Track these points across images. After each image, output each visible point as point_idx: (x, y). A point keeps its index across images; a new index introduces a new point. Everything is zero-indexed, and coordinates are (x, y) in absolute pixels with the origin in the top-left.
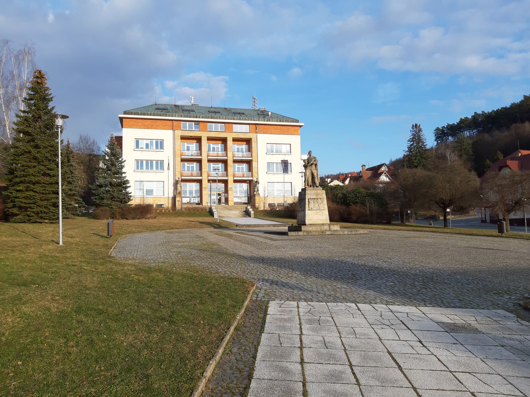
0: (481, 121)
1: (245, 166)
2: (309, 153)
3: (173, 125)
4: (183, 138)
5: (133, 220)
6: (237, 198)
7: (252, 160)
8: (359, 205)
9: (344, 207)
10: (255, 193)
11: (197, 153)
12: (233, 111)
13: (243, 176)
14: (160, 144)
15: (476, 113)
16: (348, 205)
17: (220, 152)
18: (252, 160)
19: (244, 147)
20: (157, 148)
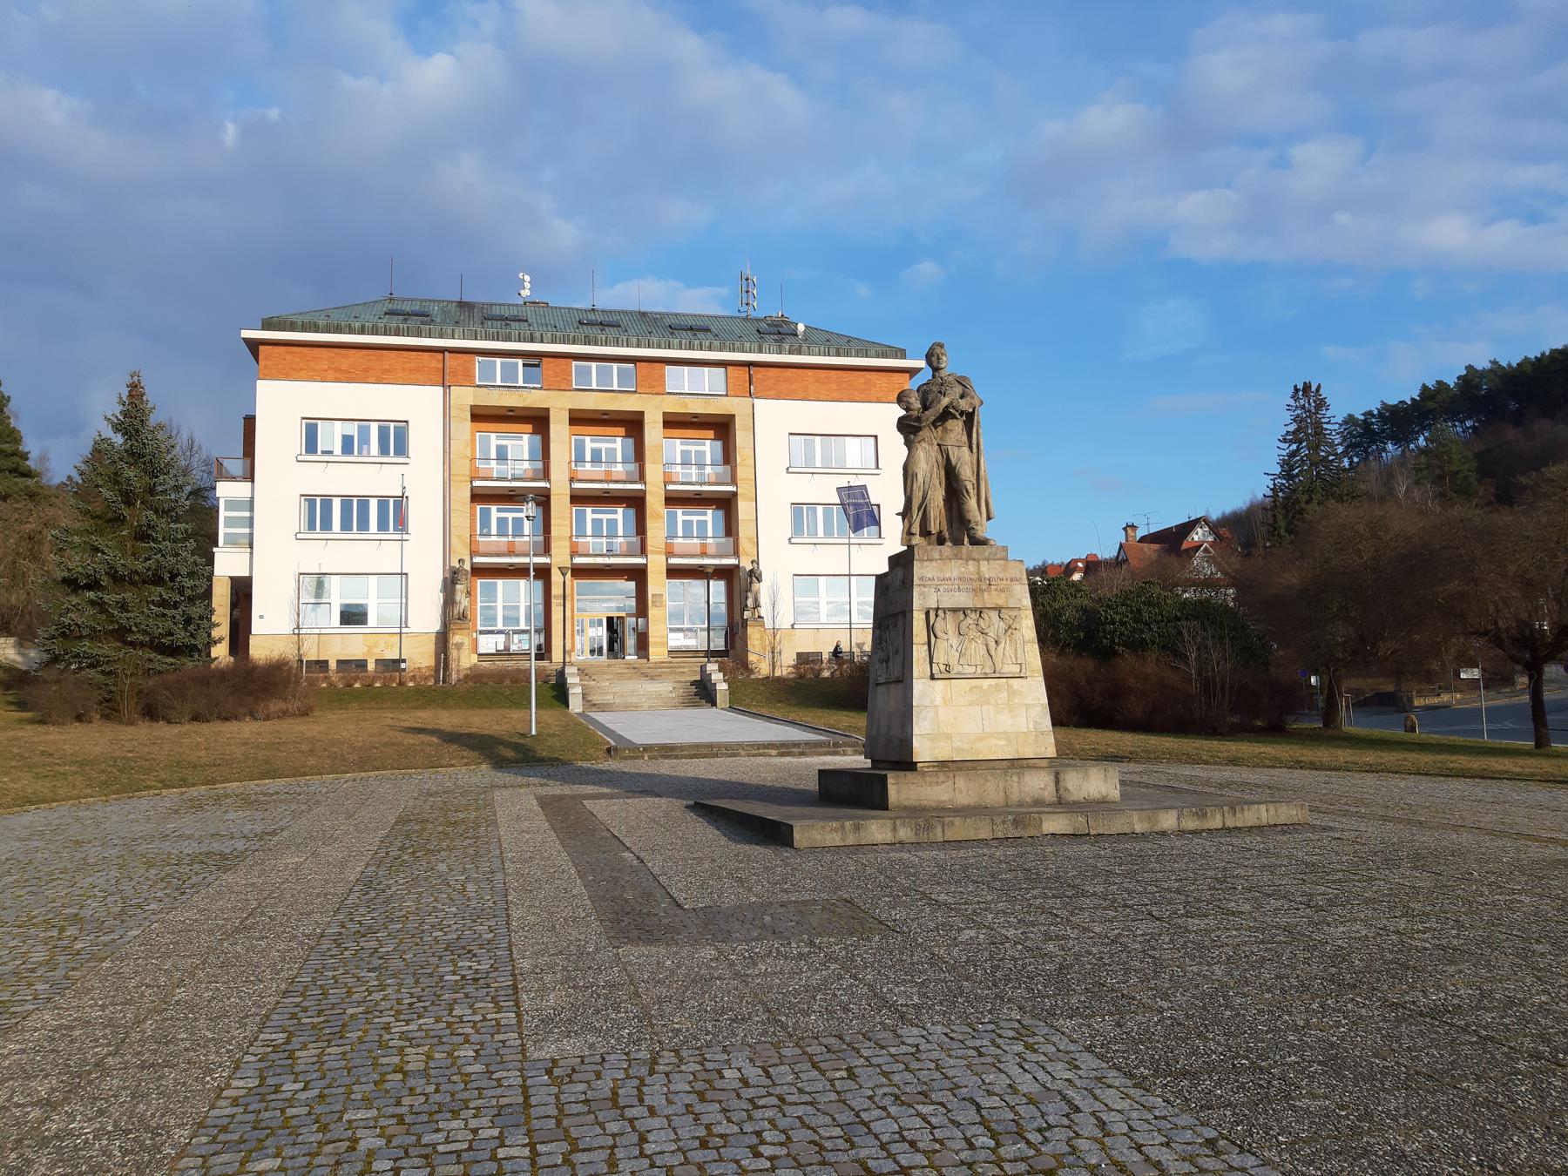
0: (1489, 390)
3: (444, 369)
4: (481, 416)
5: (196, 726)
6: (681, 635)
7: (735, 494)
9: (1089, 664)
10: (747, 614)
12: (668, 322)
13: (704, 554)
14: (395, 440)
15: (1469, 368)
16: (1106, 655)
17: (620, 467)
18: (735, 494)
19: (708, 447)
20: (384, 450)
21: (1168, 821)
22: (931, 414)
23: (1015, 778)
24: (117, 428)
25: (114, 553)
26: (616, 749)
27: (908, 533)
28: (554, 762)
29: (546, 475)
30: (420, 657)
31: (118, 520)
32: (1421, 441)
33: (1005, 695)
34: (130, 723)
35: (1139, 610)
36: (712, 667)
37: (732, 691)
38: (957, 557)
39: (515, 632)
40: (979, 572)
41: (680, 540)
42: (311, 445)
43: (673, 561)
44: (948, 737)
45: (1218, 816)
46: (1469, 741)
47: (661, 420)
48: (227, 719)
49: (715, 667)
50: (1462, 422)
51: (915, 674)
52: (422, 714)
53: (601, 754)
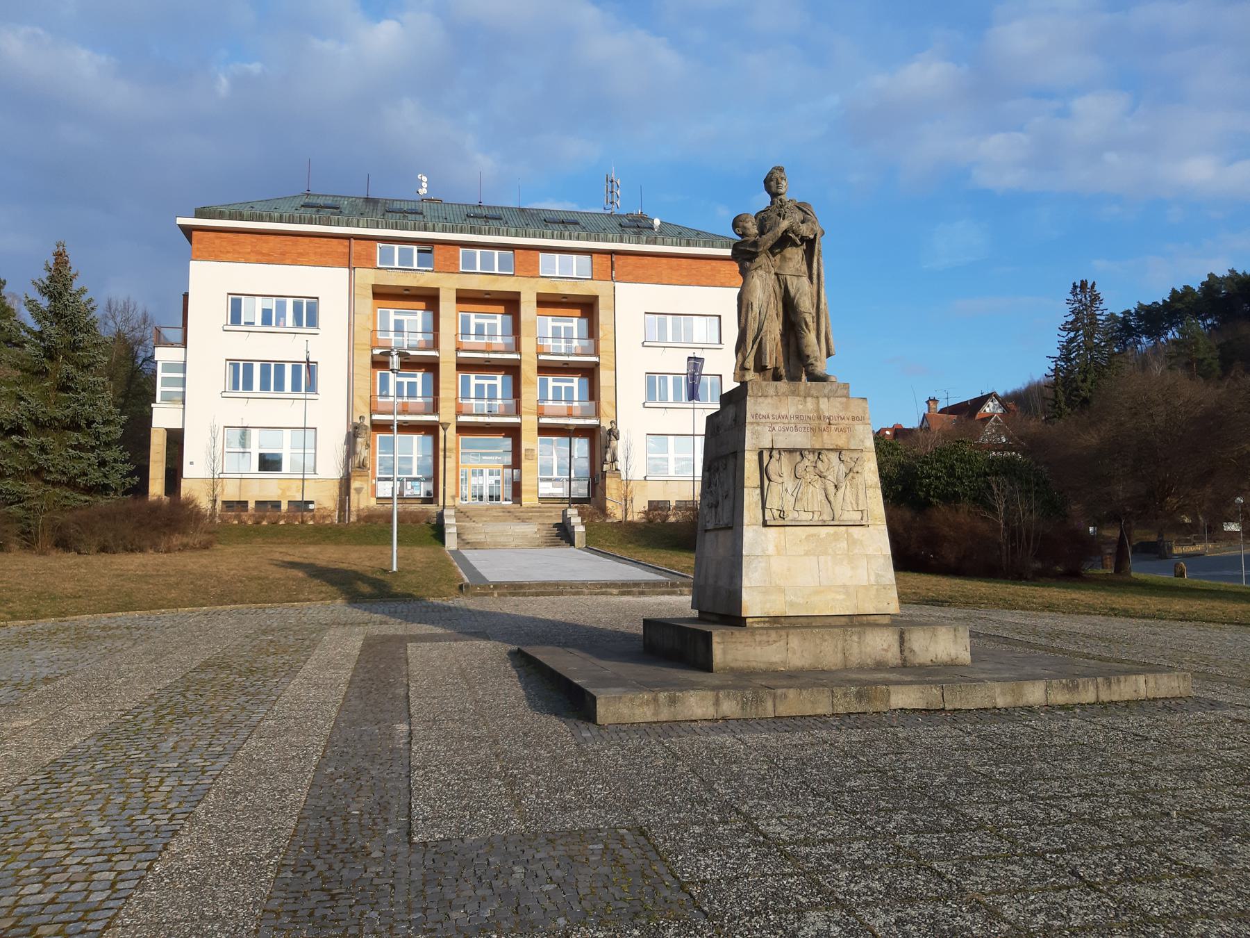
0: (1228, 294)
1: (575, 383)
2: (767, 182)
3: (349, 252)
4: (382, 294)
6: (550, 484)
7: (597, 364)
8: (965, 506)
10: (606, 467)
11: (427, 341)
12: (543, 216)
13: (570, 416)
14: (307, 313)
15: (1211, 276)
18: (597, 364)
19: (575, 323)
20: (298, 322)
21: (1035, 694)
22: (769, 239)
23: (855, 638)
24: (44, 290)
25: (37, 401)
26: (467, 586)
27: (742, 368)
28: (407, 597)
29: (435, 345)
30: (324, 498)
31: (43, 373)
32: (1170, 335)
33: (844, 545)
34: (42, 553)
35: (952, 467)
36: (572, 512)
37: (589, 534)
38: (794, 393)
39: (408, 479)
40: (818, 410)
41: (550, 403)
42: (236, 318)
43: (543, 421)
44: (781, 590)
45: (1091, 688)
46: (1224, 585)
47: (534, 299)
48: (132, 551)
49: (575, 512)
50: (1204, 320)
51: (746, 521)
52: (312, 549)
53: (454, 591)
